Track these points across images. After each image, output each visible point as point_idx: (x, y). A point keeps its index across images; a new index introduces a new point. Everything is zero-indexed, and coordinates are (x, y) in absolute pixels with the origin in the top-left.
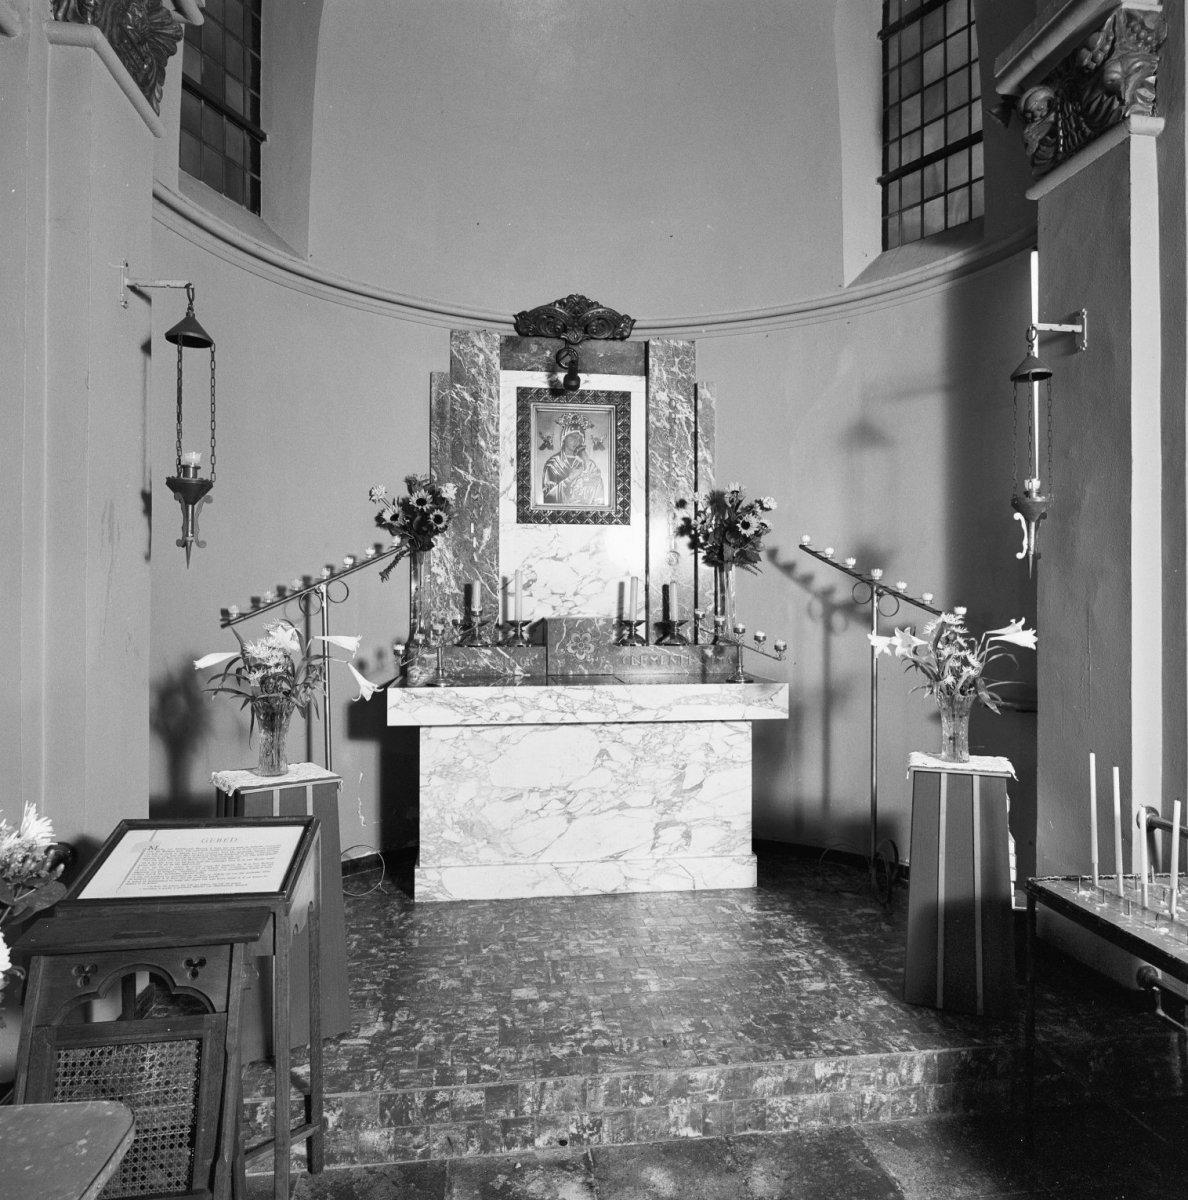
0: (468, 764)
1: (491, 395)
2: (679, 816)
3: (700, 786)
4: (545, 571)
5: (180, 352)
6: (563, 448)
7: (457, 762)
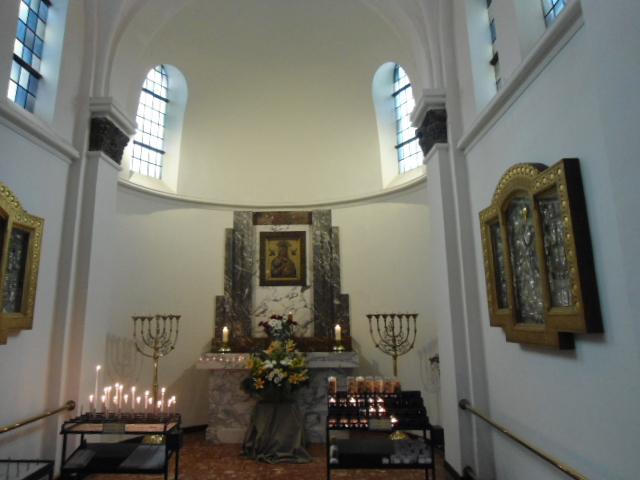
0: (228, 385)
5: (18, 468)
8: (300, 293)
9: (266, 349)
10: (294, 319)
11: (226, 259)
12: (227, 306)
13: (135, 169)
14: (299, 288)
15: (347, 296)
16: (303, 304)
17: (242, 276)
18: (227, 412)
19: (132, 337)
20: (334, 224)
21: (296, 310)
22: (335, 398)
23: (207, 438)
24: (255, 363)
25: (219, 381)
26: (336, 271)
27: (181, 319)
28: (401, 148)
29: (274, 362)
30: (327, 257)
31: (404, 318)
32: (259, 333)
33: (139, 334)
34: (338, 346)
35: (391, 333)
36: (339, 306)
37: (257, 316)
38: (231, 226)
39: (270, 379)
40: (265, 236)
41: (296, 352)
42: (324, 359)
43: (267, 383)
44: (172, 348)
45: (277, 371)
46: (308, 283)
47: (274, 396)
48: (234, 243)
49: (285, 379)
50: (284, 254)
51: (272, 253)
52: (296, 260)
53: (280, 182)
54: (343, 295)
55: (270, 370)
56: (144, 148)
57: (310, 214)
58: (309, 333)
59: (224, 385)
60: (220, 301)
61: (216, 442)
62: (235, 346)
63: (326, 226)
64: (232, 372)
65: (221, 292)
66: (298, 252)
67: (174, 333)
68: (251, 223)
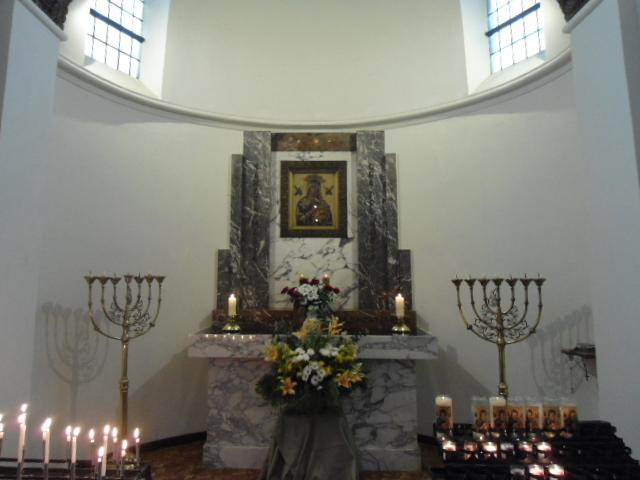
0: (236, 382)
1: (265, 165)
2: (369, 421)
3: (382, 401)
4: (296, 264)
6: (308, 193)
7: (230, 381)
8: (337, 249)
9: (295, 331)
10: (333, 284)
11: (233, 198)
12: (234, 265)
13: (98, 56)
14: (337, 241)
15: (407, 253)
16: (342, 263)
17: (255, 223)
18: (236, 422)
19: (87, 308)
20: (388, 150)
21: (332, 272)
22: (453, 440)
23: (205, 459)
24: (280, 352)
25: (223, 375)
26: (390, 216)
27: (545, 283)
28: (495, 36)
29: (311, 352)
30: (378, 196)
31: (519, 286)
32: (280, 303)
33: (97, 306)
34: (400, 325)
35: (495, 309)
36: (396, 266)
37: (277, 279)
38: (240, 151)
39: (305, 379)
40: (287, 167)
41: (344, 335)
42: (384, 346)
43: (301, 385)
44: (152, 325)
45: (315, 365)
46: (350, 235)
47: (312, 407)
48: (244, 175)
49: (328, 379)
50: (315, 193)
51: (299, 192)
52: (332, 201)
53: (314, 94)
54: (401, 251)
55: (304, 364)
56: (111, 28)
57: (353, 137)
58: (351, 304)
59: (230, 381)
60: (224, 258)
61: (218, 466)
62: (247, 325)
63: (375, 153)
64: (242, 362)
65: (225, 245)
66: (336, 191)
67: (154, 302)
68: (269, 147)
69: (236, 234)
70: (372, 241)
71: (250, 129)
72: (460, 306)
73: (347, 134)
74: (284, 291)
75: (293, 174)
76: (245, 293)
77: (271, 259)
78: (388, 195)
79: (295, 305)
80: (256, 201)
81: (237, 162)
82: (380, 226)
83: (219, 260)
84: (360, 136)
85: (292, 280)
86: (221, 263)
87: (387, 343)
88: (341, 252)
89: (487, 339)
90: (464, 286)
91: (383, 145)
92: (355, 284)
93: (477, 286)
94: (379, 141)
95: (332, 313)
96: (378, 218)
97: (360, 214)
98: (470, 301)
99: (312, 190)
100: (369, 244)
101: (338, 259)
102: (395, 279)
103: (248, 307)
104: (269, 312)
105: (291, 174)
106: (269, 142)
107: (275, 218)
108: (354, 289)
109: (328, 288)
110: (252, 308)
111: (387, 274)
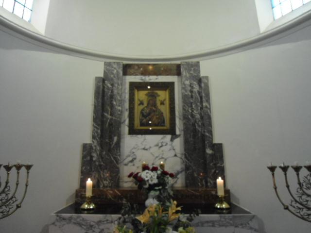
1: (118, 85)
4: (140, 154)
8: (169, 143)
10: (166, 169)
12: (94, 155)
14: (169, 137)
16: (173, 153)
17: (111, 125)
26: (206, 119)
30: (197, 105)
32: (128, 184)
36: (211, 155)
37: (126, 165)
38: (102, 75)
40: (134, 86)
44: (18, 207)
46: (178, 132)
48: (103, 91)
51: (141, 103)
52: (165, 110)
57: (179, 66)
58: (179, 183)
65: (88, 140)
66: (167, 102)
68: (121, 73)
69: (97, 132)
70: (194, 136)
71: (108, 61)
72: (276, 188)
73: (175, 64)
74: (130, 176)
75: (138, 90)
76: (102, 176)
77: (121, 149)
78: (204, 104)
79: (138, 187)
80: (111, 109)
81: (99, 82)
82: (199, 126)
83: (83, 151)
84: (183, 65)
85: (137, 165)
86: (84, 153)
87: (216, 221)
88: (171, 145)
89: (303, 219)
90: (278, 171)
91: (200, 71)
92: (182, 168)
93: (291, 172)
94: (197, 68)
95: (169, 198)
96: (197, 120)
97: (185, 117)
98: (285, 184)
99: (151, 102)
100: (192, 139)
101: (170, 150)
102: (211, 164)
103: (104, 186)
104: (119, 191)
105: (136, 91)
106: (122, 69)
107: (125, 121)
108: (181, 172)
109: (165, 173)
110: (107, 187)
111: (205, 161)
